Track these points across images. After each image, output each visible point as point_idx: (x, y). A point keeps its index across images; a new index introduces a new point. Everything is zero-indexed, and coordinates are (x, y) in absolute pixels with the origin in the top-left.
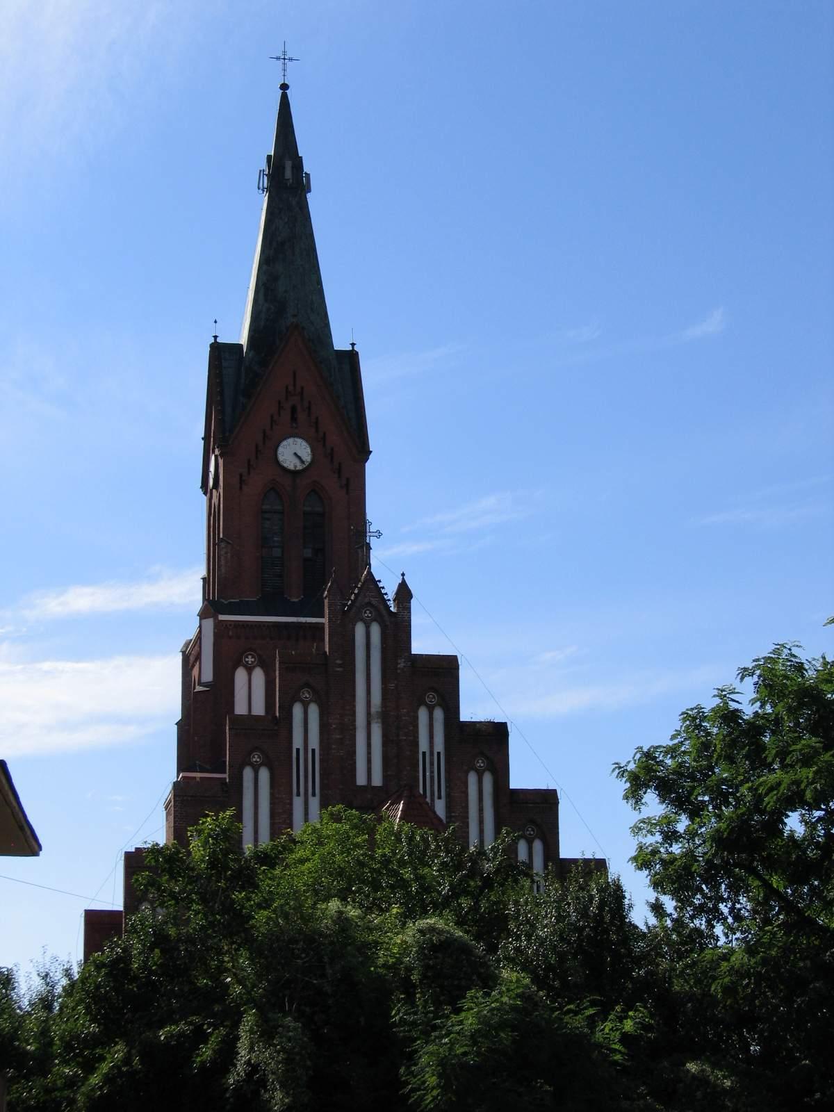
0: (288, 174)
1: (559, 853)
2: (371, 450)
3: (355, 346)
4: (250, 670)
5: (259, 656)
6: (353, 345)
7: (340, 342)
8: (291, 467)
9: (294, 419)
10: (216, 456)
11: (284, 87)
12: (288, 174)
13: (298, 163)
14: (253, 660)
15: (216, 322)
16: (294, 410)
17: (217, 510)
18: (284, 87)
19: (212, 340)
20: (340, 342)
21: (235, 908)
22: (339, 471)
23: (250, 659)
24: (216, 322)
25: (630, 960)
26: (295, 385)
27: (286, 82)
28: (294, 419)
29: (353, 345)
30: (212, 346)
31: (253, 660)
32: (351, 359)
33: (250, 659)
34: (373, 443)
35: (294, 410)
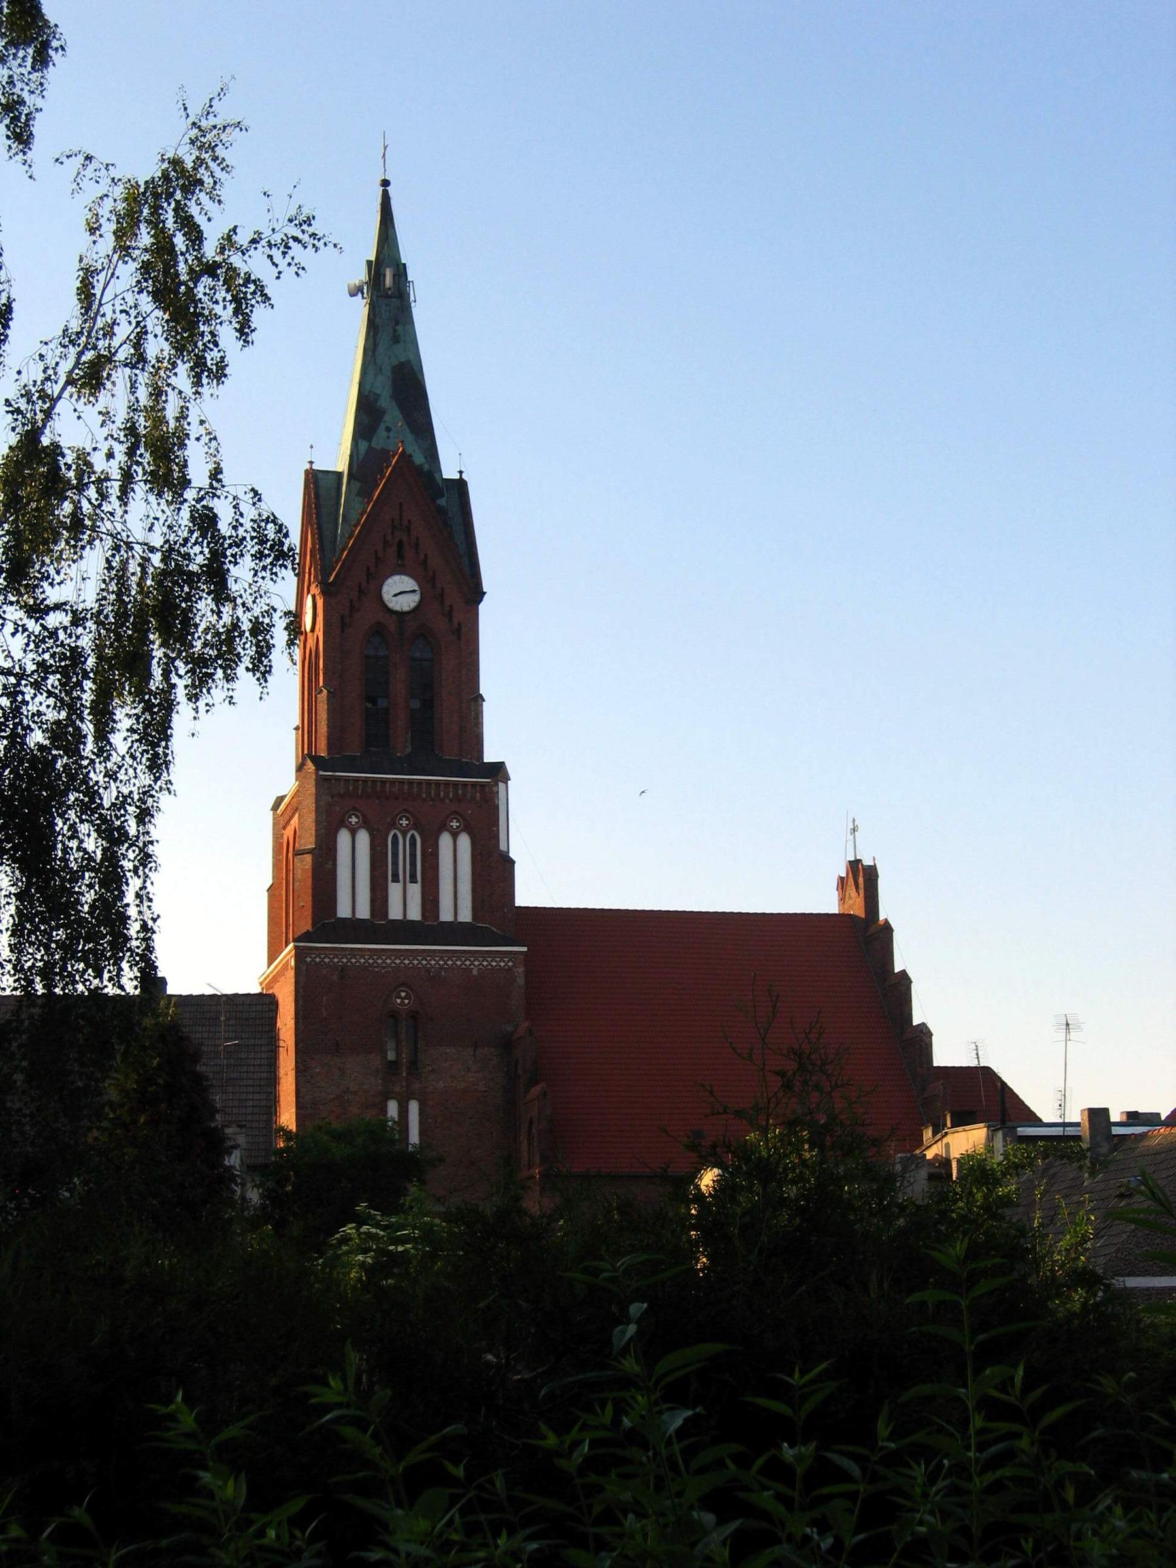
0: (388, 281)
1: (1028, 1108)
2: (484, 591)
3: (463, 474)
4: (455, 835)
5: (364, 817)
6: (461, 472)
7: (449, 472)
8: (413, 605)
9: (400, 556)
10: (314, 597)
11: (385, 183)
12: (388, 281)
13: (401, 272)
14: (458, 824)
15: (312, 447)
16: (400, 545)
17: (313, 654)
18: (385, 183)
19: (308, 466)
20: (449, 472)
21: (1076, 1291)
22: (449, 615)
23: (354, 820)
24: (312, 447)
25: (23, 977)
26: (401, 519)
27: (387, 178)
28: (400, 556)
29: (461, 472)
30: (307, 472)
31: (458, 824)
32: (460, 487)
33: (404, 822)
34: (486, 586)
35: (400, 545)
